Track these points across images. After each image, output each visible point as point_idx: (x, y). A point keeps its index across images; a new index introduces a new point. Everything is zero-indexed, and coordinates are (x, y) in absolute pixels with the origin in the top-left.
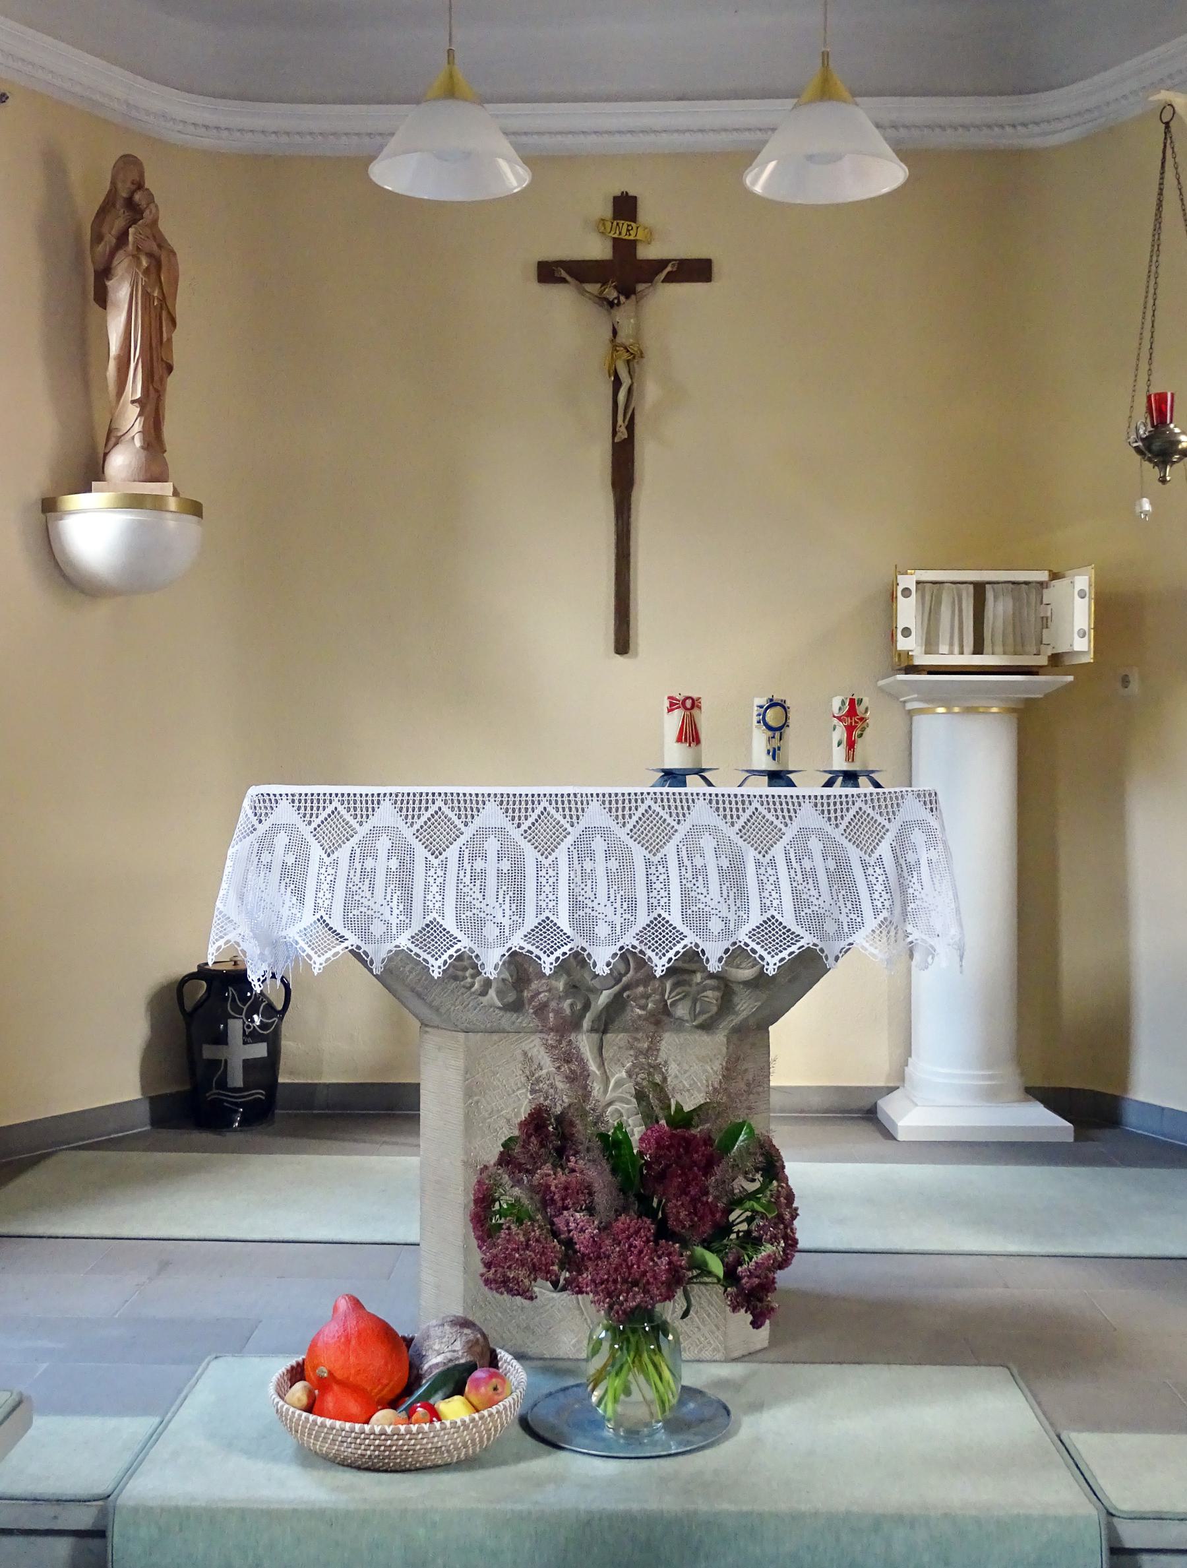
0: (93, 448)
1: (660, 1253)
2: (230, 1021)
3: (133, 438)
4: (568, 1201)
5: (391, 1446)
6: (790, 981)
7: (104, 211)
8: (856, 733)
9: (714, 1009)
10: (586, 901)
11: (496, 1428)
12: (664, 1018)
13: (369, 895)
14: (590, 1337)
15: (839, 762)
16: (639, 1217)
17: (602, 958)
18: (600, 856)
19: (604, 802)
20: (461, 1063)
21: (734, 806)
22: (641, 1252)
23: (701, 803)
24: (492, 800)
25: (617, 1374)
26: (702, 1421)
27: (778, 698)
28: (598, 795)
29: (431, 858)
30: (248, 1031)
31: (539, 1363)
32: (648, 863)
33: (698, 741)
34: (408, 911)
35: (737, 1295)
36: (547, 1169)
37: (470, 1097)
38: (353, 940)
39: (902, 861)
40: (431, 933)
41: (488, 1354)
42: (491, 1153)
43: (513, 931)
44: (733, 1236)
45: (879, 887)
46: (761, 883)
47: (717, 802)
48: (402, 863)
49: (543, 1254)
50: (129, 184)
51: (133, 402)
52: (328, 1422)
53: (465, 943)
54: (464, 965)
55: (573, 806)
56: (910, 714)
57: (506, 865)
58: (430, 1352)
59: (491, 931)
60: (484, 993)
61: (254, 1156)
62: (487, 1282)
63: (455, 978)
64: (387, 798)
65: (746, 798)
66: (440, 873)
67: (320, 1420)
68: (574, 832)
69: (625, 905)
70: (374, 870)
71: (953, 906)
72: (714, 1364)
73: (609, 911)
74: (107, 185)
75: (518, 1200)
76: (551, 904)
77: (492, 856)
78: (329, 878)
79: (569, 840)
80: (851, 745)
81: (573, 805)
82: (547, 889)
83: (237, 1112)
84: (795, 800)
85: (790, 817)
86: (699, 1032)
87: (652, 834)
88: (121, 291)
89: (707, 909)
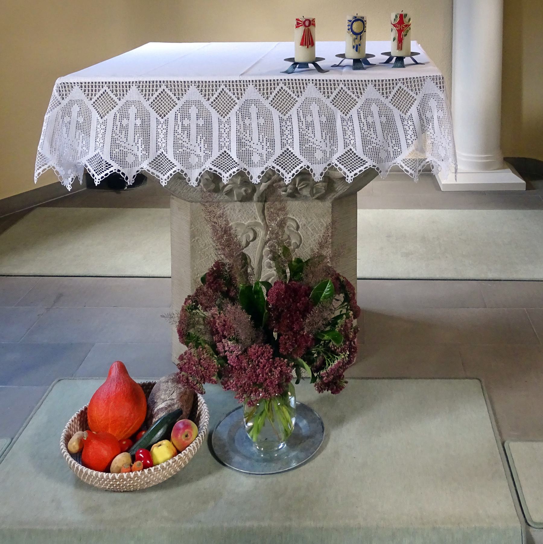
1: (276, 365)
18: (254, 116)
20: (189, 219)
22: (264, 366)
25: (261, 415)
28: (253, 81)
29: (160, 118)
32: (281, 120)
39: (423, 117)
40: (159, 162)
45: (410, 132)
46: (344, 131)
48: (143, 121)
57: (201, 122)
58: (158, 401)
59: (194, 160)
65: (336, 82)
66: (164, 127)
69: (268, 144)
73: (259, 147)
76: (227, 144)
77: (193, 116)
79: (237, 107)
82: (225, 135)
86: (316, 201)
87: (283, 103)
89: (314, 146)
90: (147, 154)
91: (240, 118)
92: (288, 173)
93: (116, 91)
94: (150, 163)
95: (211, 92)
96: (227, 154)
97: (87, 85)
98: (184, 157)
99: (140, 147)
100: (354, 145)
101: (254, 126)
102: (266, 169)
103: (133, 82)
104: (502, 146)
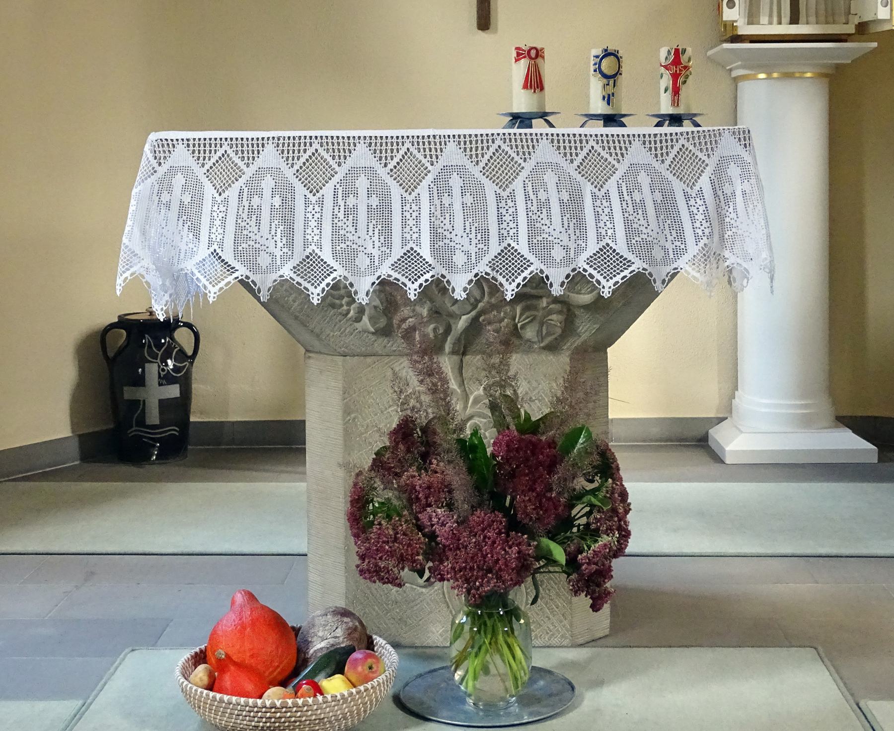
1: (510, 543)
2: (147, 365)
4: (431, 499)
5: (280, 718)
6: (624, 305)
8: (681, 80)
9: (559, 331)
10: (445, 233)
11: (371, 701)
12: (514, 339)
13: (255, 229)
14: (453, 622)
15: (666, 107)
16: (493, 511)
17: (459, 285)
18: (457, 191)
19: (459, 143)
21: (573, 144)
22: (494, 542)
23: (544, 142)
24: (362, 142)
25: (476, 656)
26: (550, 695)
27: (611, 48)
29: (310, 196)
30: (162, 374)
31: (411, 651)
32: (499, 198)
33: (542, 89)
34: (290, 244)
35: (578, 581)
36: (413, 471)
37: (349, 414)
38: (242, 271)
39: (720, 193)
40: (310, 264)
41: (366, 640)
42: (366, 460)
43: (382, 260)
44: (575, 530)
45: (700, 217)
46: (597, 215)
47: (558, 142)
49: (409, 545)
52: (226, 698)
53: (340, 272)
54: (340, 292)
55: (433, 147)
56: (736, 80)
57: (375, 201)
58: (315, 639)
59: (363, 261)
60: (358, 320)
61: (169, 484)
62: (362, 572)
63: (333, 306)
64: (270, 142)
65: (583, 138)
66: (317, 209)
67: (218, 696)
68: (434, 170)
70: (259, 207)
71: (764, 231)
72: (561, 649)
75: (389, 499)
76: (415, 236)
77: (362, 192)
78: (221, 215)
79: (430, 177)
80: (676, 91)
81: (432, 146)
82: (411, 222)
83: (154, 446)
84: (626, 138)
85: (622, 155)
86: (546, 352)
87: (501, 171)
89: (550, 238)
90: (290, 253)
91: (435, 195)
92: (510, 284)
93: (243, 152)
94: (294, 268)
95: (389, 154)
96: (415, 252)
97: (197, 142)
98: (348, 257)
99: (279, 241)
100: (614, 238)
101: (457, 207)
102: (475, 276)
103: (268, 138)
104: (832, 390)
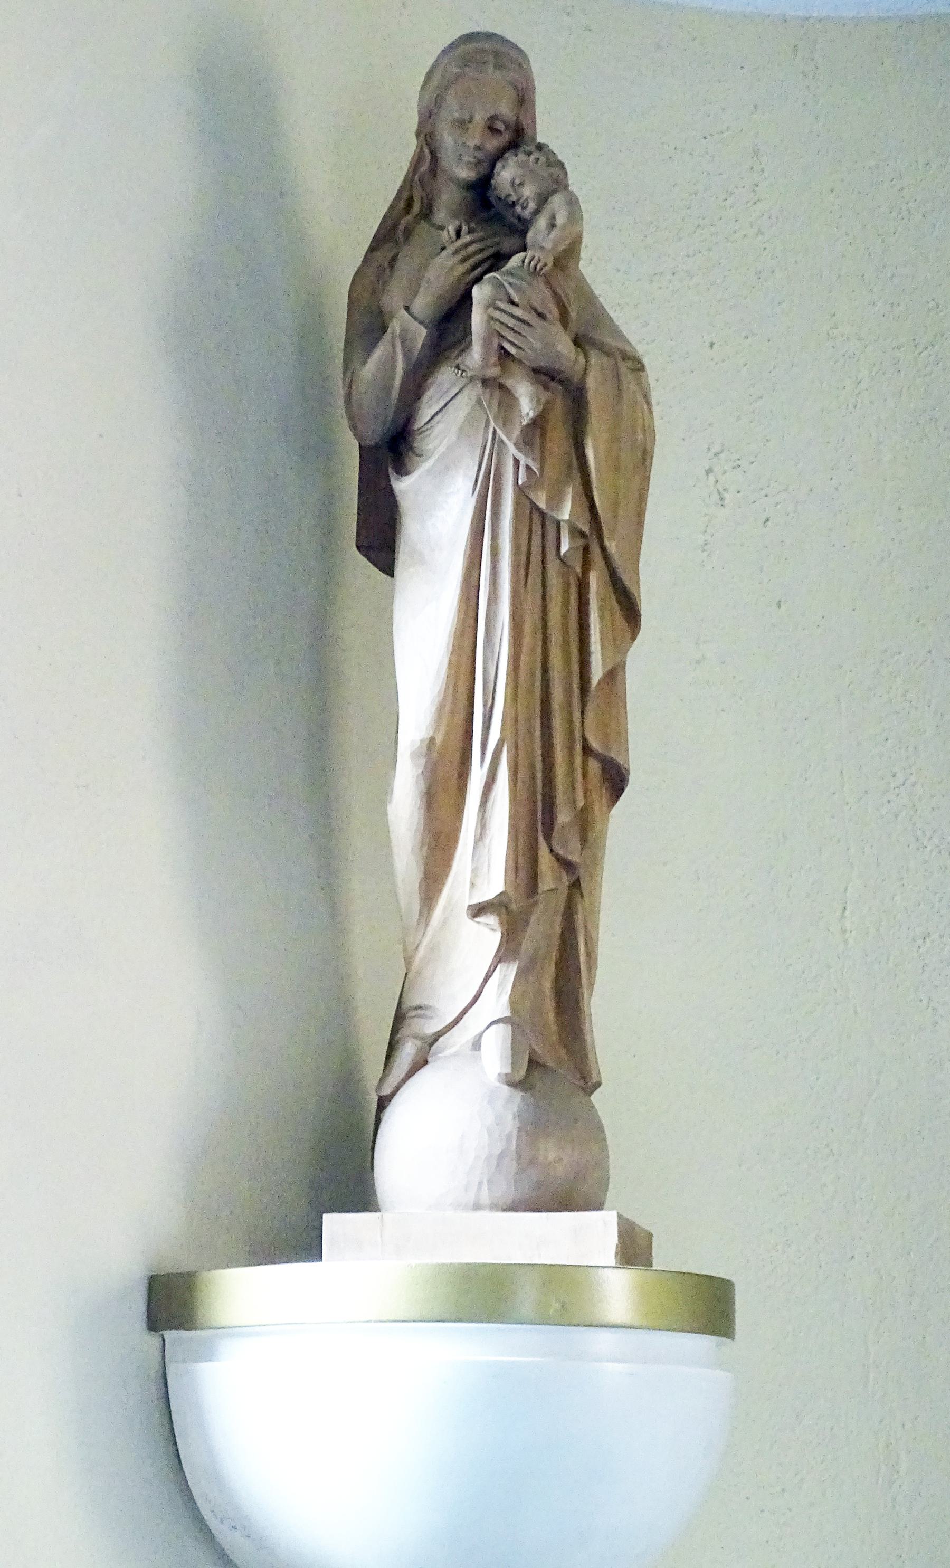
0: (346, 1084)
3: (477, 1044)
7: (390, 237)
50: (475, 136)
51: (478, 911)
74: (412, 145)
88: (441, 504)
